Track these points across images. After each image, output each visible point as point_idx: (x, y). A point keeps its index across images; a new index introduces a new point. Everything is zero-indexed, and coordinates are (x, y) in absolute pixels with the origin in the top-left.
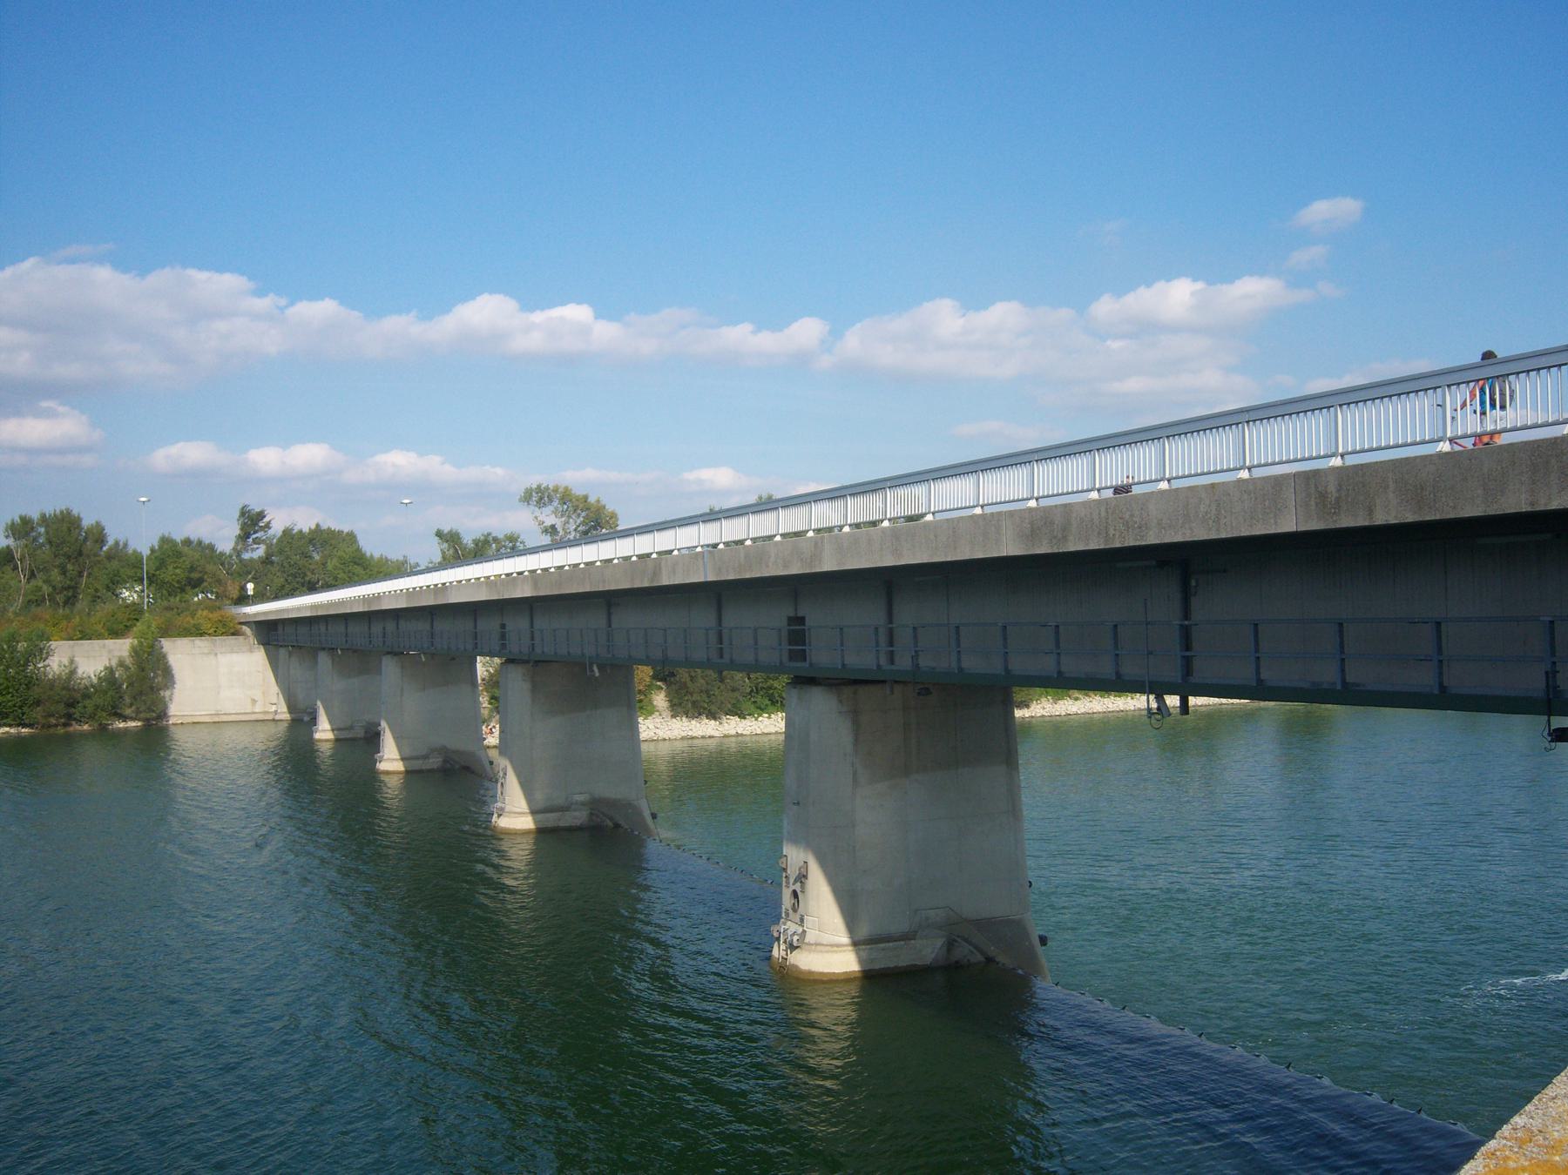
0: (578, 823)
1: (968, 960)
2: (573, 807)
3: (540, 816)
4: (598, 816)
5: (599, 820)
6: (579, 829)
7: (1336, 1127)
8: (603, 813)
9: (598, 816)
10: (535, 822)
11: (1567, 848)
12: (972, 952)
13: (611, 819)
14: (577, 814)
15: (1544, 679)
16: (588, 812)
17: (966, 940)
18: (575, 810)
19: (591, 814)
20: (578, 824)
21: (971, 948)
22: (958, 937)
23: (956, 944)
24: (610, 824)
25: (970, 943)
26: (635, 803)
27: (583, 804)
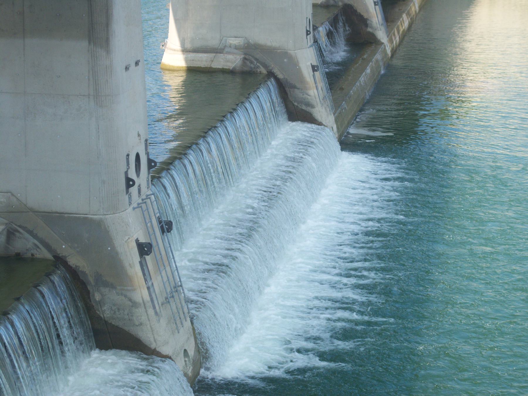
0: (230, 66)
1: (33, 255)
2: (227, 50)
3: (192, 55)
4: (251, 62)
5: (252, 66)
6: (232, 72)
7: (462, 383)
8: (257, 59)
9: (251, 62)
10: (186, 60)
11: (526, 147)
12: (36, 245)
13: (265, 66)
14: (230, 57)
15: (48, 211)
16: (243, 56)
17: (31, 233)
18: (229, 53)
19: (245, 59)
20: (231, 68)
21: (36, 242)
22: (20, 226)
23: (17, 234)
24: (264, 71)
25: (35, 236)
26: (292, 52)
27: (236, 48)
